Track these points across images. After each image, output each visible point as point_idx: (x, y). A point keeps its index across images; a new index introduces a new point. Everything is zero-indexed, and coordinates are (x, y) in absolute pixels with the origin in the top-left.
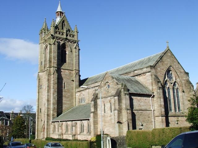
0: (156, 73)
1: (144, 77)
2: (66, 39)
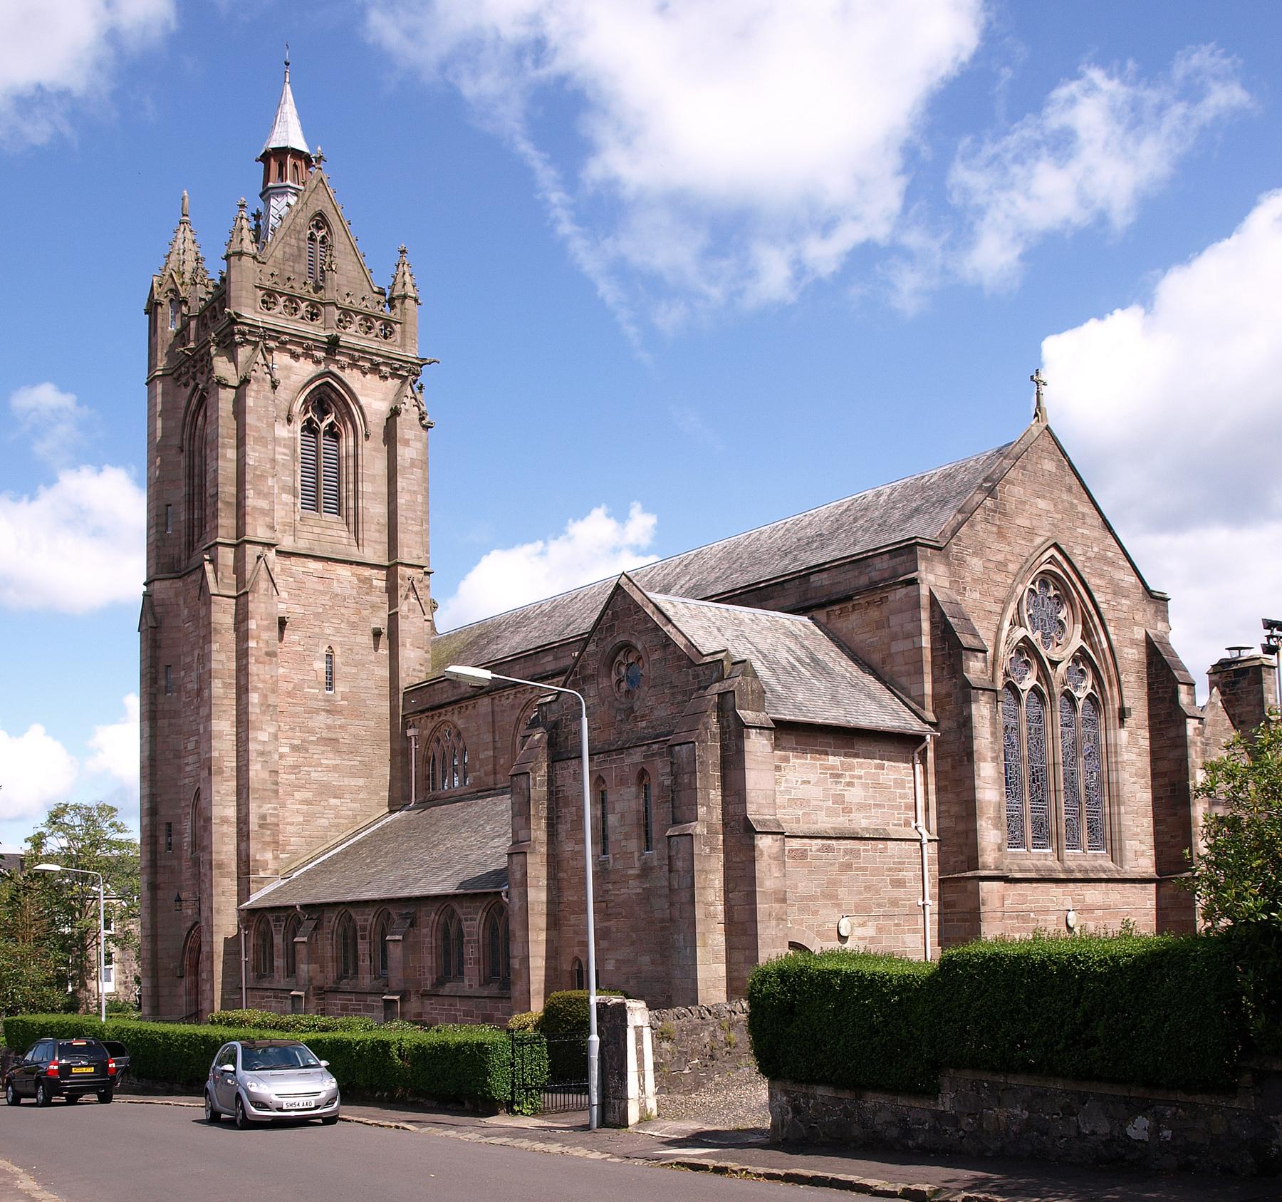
0: (958, 593)
1: (874, 614)
2: (333, 346)
